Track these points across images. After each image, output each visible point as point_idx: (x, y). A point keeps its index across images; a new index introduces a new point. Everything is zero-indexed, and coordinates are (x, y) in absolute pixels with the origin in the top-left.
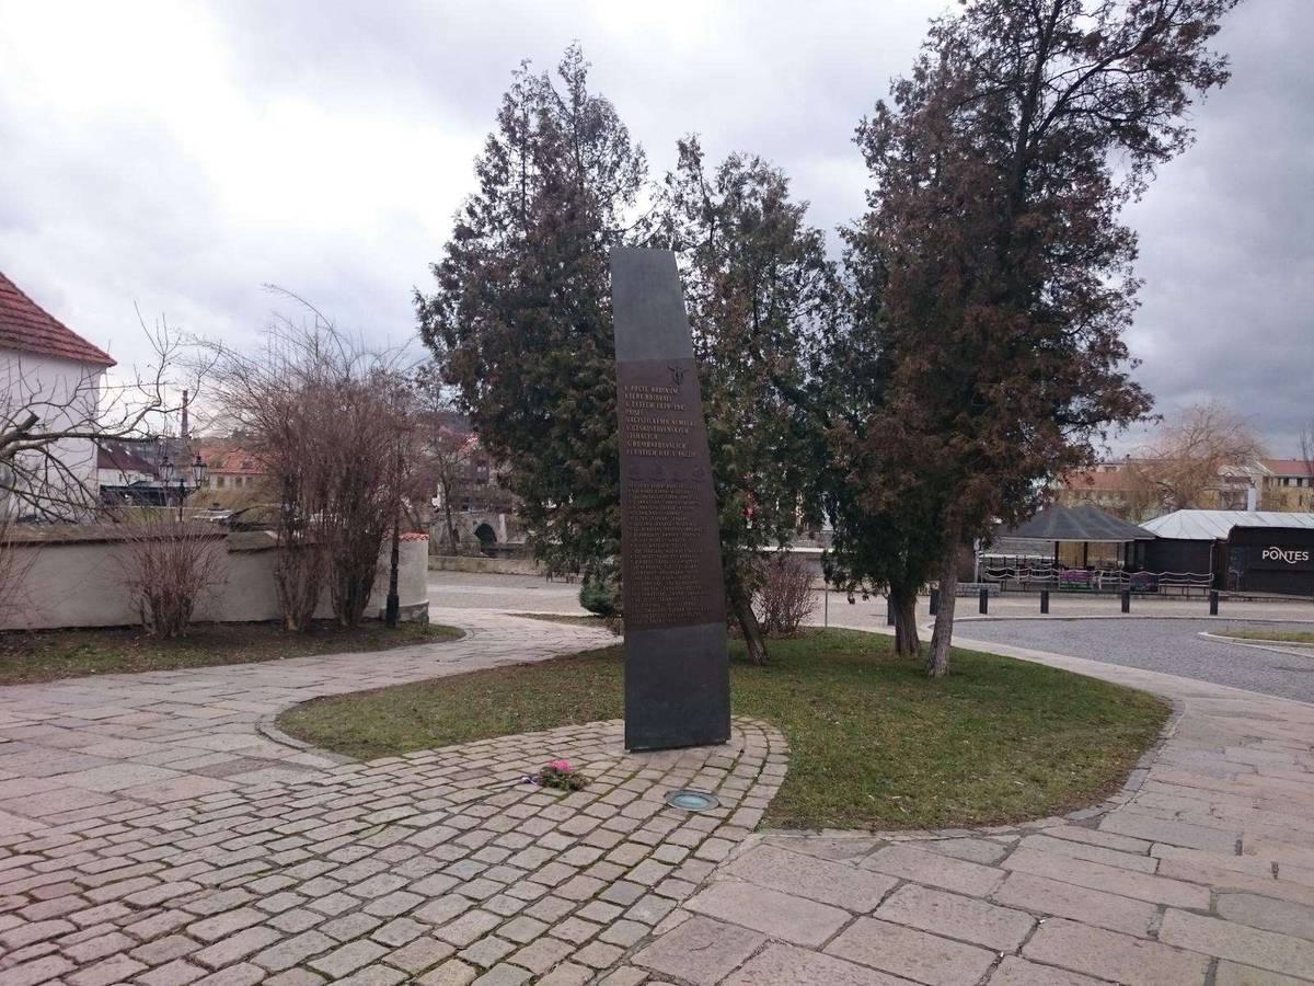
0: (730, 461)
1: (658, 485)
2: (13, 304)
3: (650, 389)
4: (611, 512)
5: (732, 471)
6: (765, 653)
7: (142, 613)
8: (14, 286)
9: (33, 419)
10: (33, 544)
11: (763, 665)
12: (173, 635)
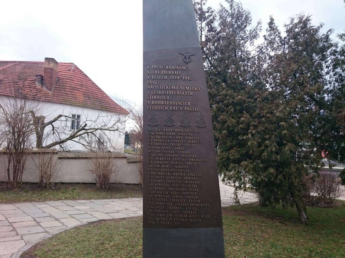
0: (284, 130)
1: (169, 130)
2: (107, 100)
3: (164, 67)
4: (232, 152)
5: (285, 134)
6: (308, 218)
7: (96, 180)
8: (107, 95)
9: (86, 125)
10: (68, 158)
11: (306, 224)
12: (103, 187)
